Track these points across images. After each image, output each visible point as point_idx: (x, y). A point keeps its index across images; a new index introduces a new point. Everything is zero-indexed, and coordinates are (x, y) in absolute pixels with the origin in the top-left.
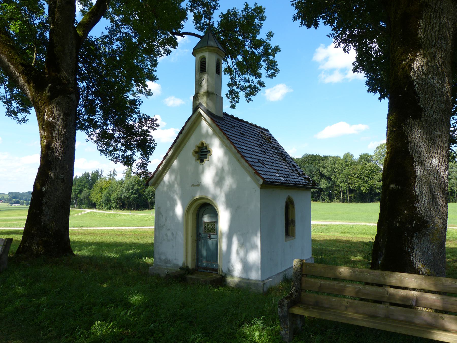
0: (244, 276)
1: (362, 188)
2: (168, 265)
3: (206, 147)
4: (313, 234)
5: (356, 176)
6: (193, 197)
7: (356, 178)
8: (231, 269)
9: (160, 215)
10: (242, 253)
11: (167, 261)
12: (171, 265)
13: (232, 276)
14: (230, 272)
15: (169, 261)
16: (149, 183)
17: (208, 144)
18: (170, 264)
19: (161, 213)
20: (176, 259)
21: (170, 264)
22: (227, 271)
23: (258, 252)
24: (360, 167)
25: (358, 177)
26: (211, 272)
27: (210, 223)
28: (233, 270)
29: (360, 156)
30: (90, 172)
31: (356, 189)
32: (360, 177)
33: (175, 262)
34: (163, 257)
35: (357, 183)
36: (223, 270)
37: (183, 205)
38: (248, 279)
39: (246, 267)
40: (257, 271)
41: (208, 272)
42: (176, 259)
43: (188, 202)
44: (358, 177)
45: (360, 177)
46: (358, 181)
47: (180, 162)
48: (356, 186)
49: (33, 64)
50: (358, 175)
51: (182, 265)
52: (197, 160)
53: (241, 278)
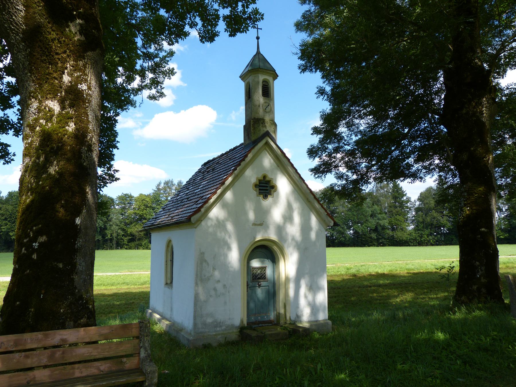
0: (313, 319)
1: (11, 234)
2: (218, 329)
3: (269, 182)
4: (95, 288)
5: (3, 218)
6: (255, 238)
7: (4, 220)
8: (299, 314)
9: (204, 264)
10: (310, 297)
11: (217, 324)
12: (224, 328)
13: (301, 322)
14: (298, 317)
15: (220, 323)
16: (192, 219)
17: (272, 178)
18: (221, 326)
19: (206, 261)
20: (230, 319)
21: (221, 326)
22: (295, 318)
23: (324, 292)
24: (10, 208)
25: (6, 219)
26: (264, 325)
27: (259, 268)
28: (302, 315)
29: (9, 193)
30: (135, 194)
31: (2, 234)
32: (9, 219)
33: (229, 323)
34: (209, 320)
35: (4, 227)
36: (291, 318)
37: (240, 248)
38: (317, 321)
39: (314, 308)
40: (324, 311)
41: (260, 326)
42: (230, 319)
43: (248, 245)
44: (6, 219)
45: (9, 219)
46: (6, 224)
47: (235, 194)
48: (3, 230)
49: (354, 46)
50: (7, 217)
51: (240, 324)
52: (259, 195)
53: (309, 322)
